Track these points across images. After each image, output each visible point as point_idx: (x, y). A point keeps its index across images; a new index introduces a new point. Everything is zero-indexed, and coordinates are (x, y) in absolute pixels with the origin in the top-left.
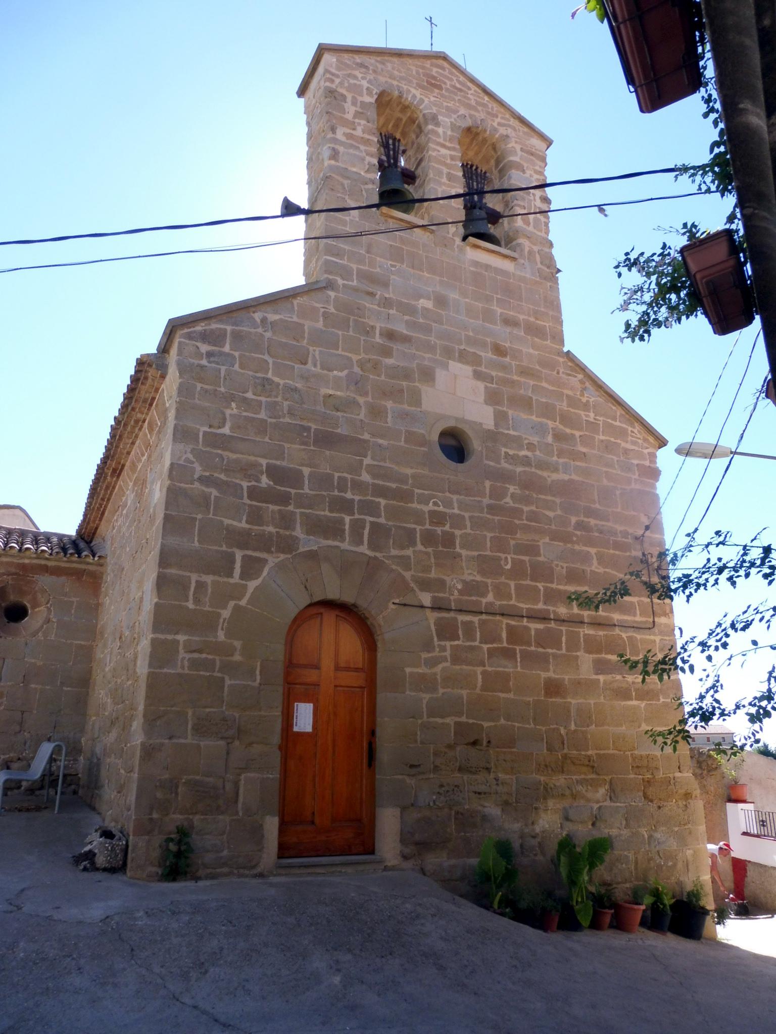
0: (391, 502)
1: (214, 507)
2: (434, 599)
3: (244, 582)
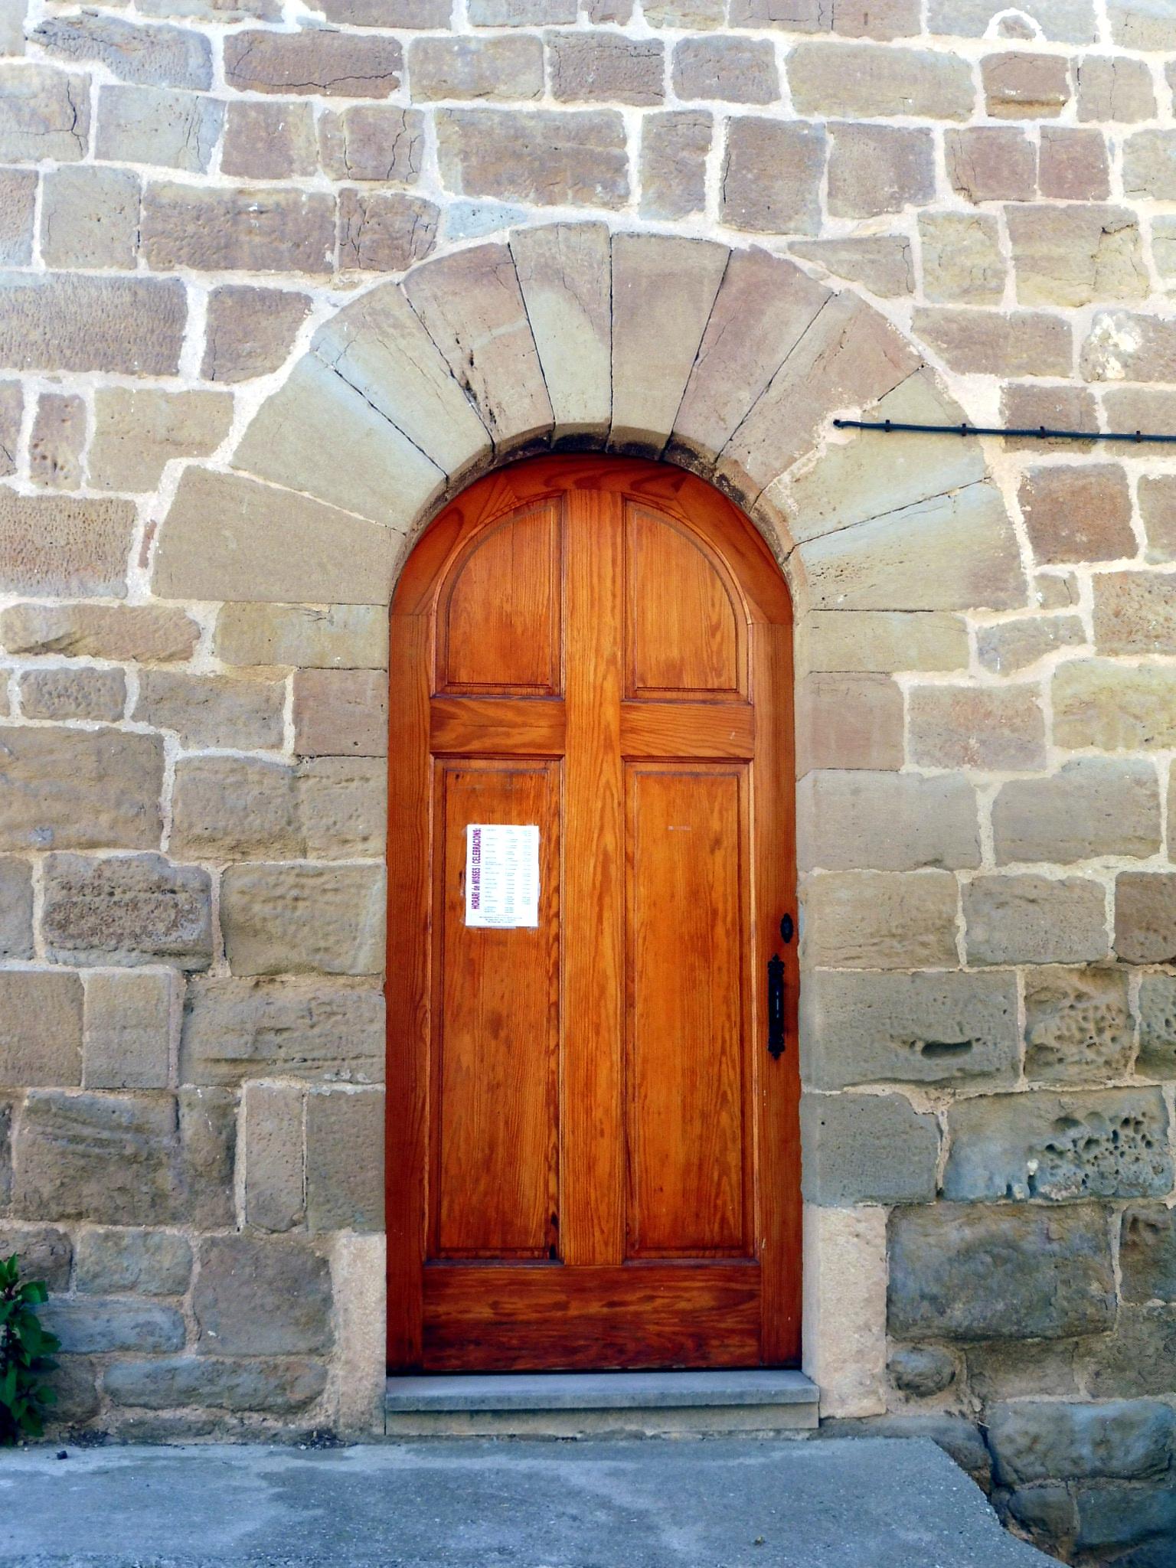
0: (818, 38)
1: (102, 128)
2: (1016, 397)
3: (219, 387)
